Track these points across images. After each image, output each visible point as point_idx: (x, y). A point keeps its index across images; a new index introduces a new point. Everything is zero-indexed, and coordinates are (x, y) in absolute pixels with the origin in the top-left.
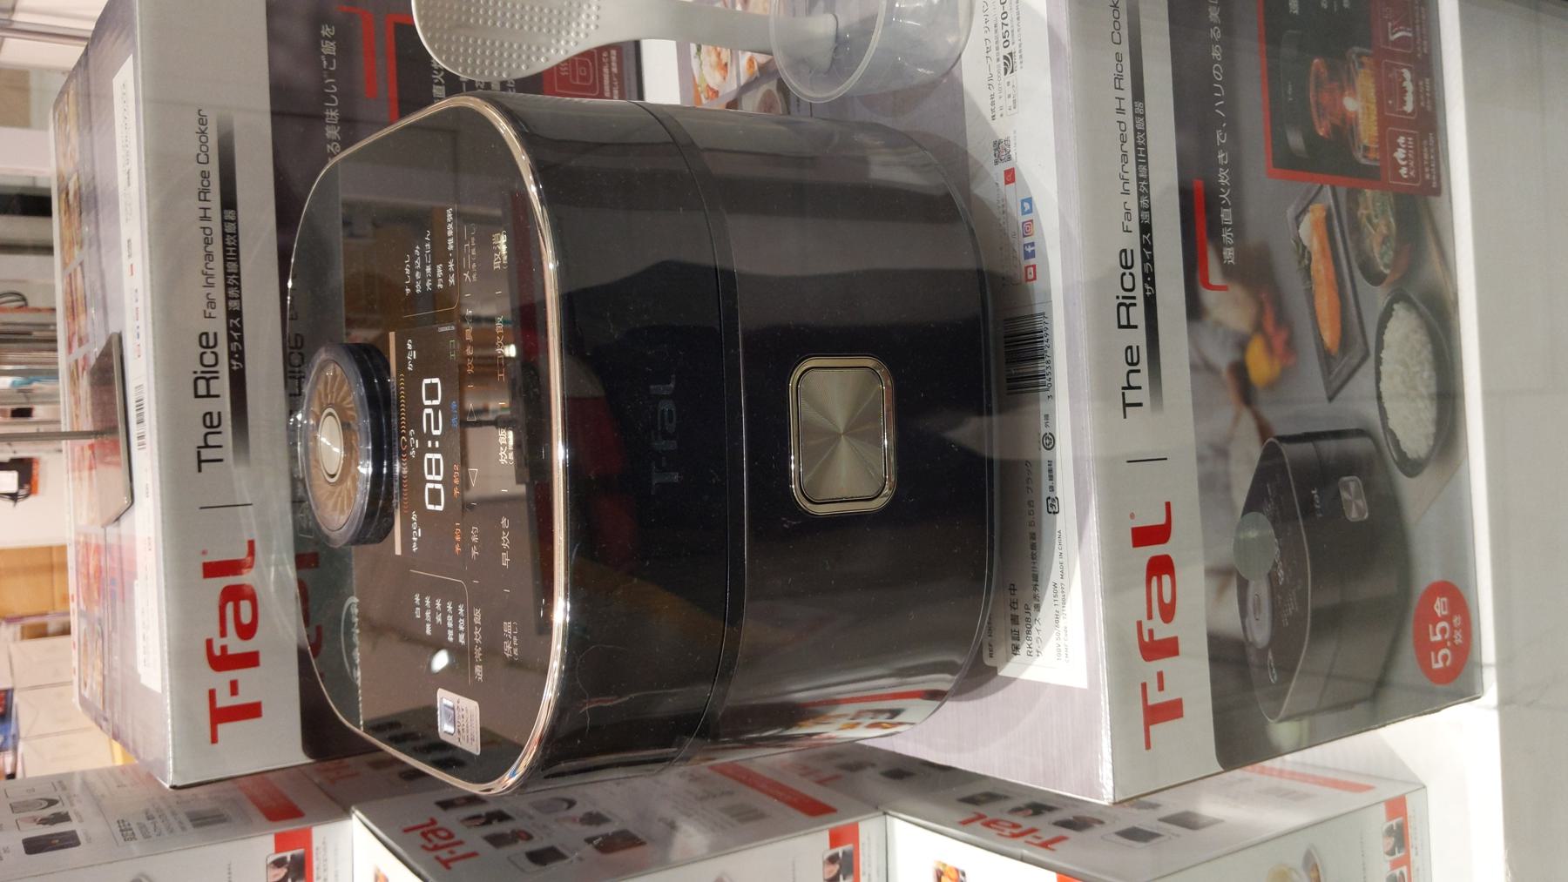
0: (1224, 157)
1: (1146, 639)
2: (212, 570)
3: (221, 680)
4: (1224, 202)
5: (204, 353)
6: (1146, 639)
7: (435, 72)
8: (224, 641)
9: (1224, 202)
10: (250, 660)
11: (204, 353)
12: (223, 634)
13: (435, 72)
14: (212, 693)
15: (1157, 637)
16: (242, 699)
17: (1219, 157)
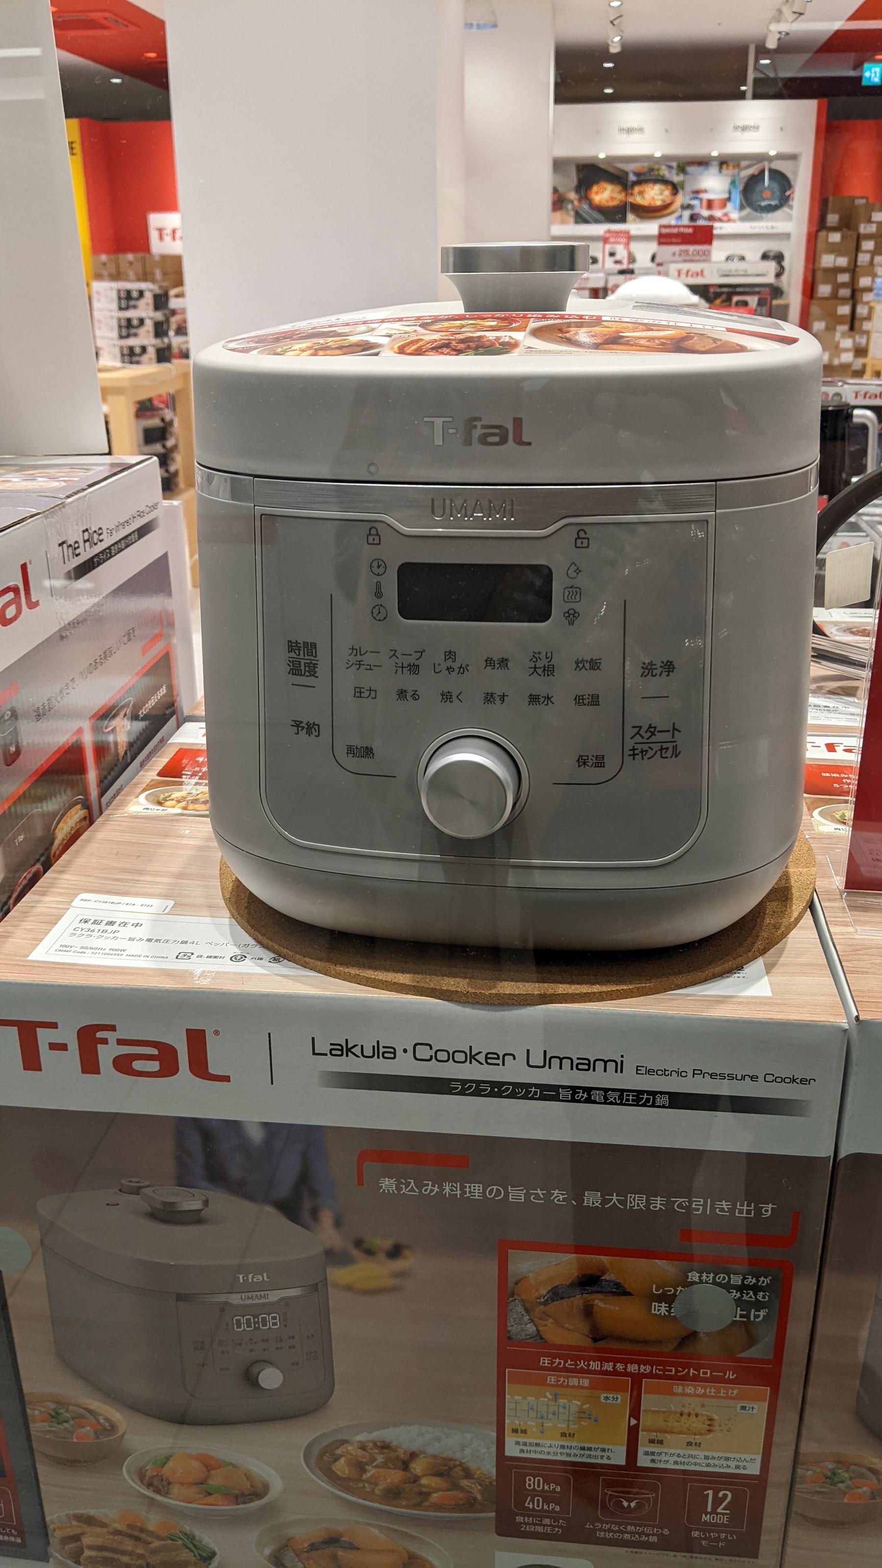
0: (722, 1210)
1: (100, 1035)
2: (196, 1039)
3: (68, 1035)
4: (579, 1363)
5: (431, 1048)
6: (100, 1035)
7: (586, 1363)
8: (112, 1042)
9: (579, 1363)
10: (90, 1065)
11: (431, 1048)
12: (120, 1042)
13: (586, 1363)
14: (54, 1025)
15: (100, 1047)
16: (45, 1054)
17: (724, 1203)
